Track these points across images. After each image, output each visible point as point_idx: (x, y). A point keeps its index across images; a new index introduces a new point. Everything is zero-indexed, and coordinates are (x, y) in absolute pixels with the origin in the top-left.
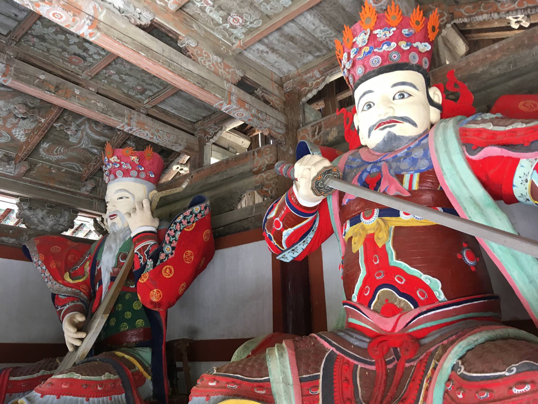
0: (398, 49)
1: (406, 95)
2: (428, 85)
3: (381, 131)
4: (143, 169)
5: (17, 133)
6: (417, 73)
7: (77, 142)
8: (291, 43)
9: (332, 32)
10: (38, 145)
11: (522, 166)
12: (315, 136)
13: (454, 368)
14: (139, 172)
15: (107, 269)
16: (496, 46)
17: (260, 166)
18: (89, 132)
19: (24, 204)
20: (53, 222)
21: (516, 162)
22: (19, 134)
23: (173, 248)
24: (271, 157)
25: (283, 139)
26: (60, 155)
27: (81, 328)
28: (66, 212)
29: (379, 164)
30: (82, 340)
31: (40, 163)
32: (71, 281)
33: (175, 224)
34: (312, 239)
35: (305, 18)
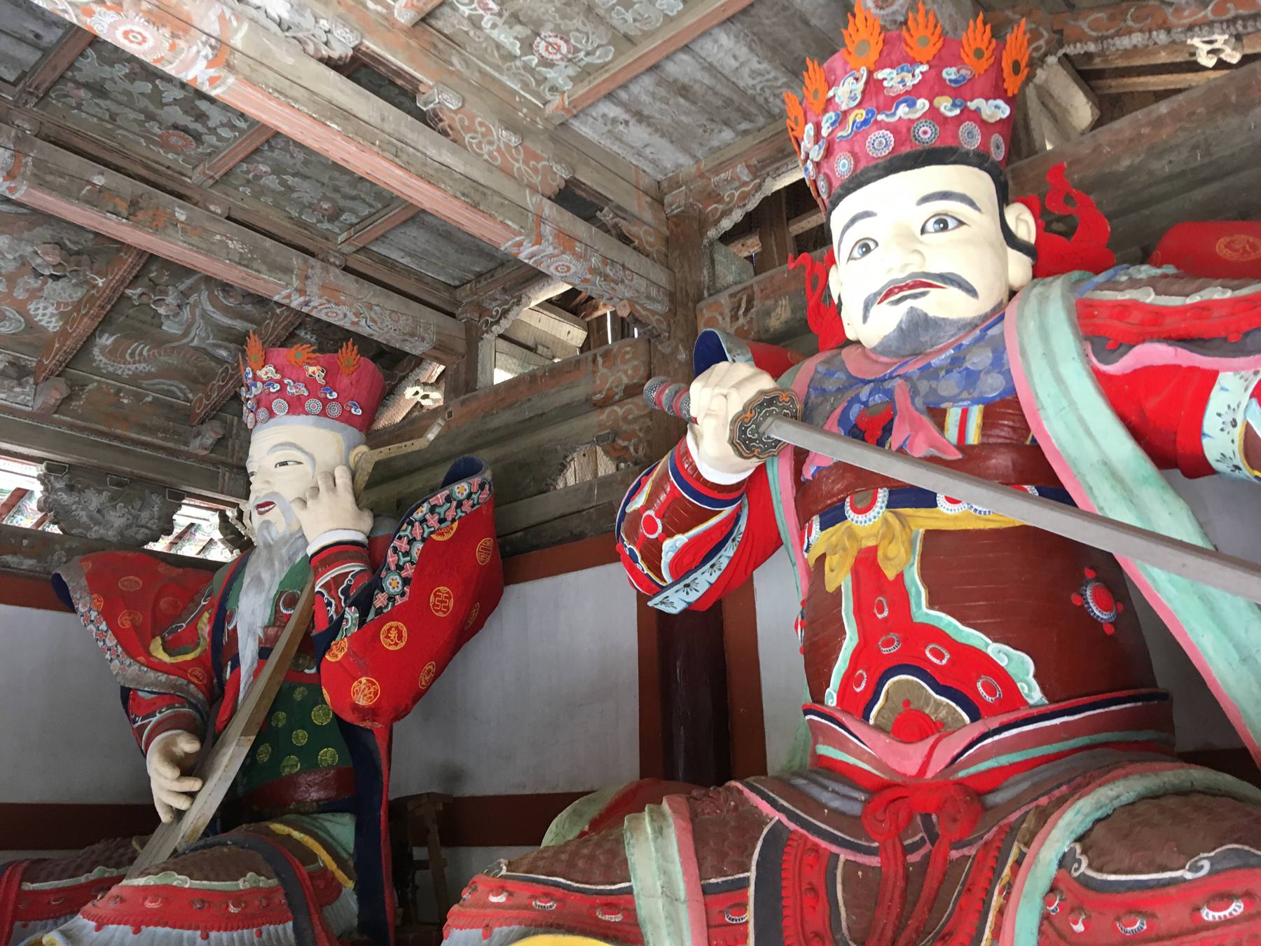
0: (933, 114)
1: (951, 224)
2: (1004, 199)
3: (894, 307)
4: (335, 395)
5: (40, 312)
6: (976, 170)
7: (179, 332)
8: (682, 101)
9: (779, 75)
10: (90, 340)
11: (1222, 389)
12: (737, 319)
13: (1065, 862)
14: (325, 402)
15: (251, 631)
16: (1163, 108)
17: (610, 389)
18: (209, 308)
19: (56, 478)
20: (123, 520)
21: (1209, 379)
22: (44, 315)
23: (406, 581)
24: (635, 369)
25: (664, 326)
26: (140, 362)
27: (190, 767)
28: (154, 497)
29: (888, 385)
30: (192, 795)
31: (93, 381)
32: (165, 658)
33: (411, 523)
34: (732, 560)
35: (716, 41)
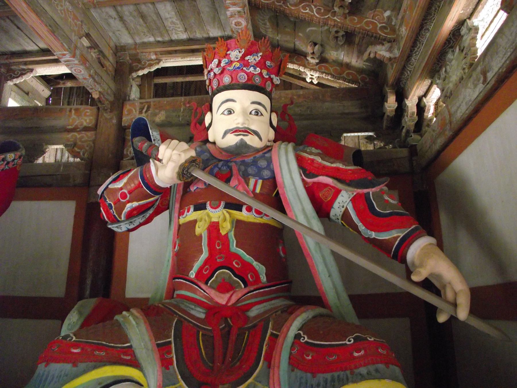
0: (261, 74)
1: (260, 114)
8: (141, 20)
9: (181, 27)
12: (142, 113)
13: (297, 337)
16: (301, 92)
17: (76, 126)
21: (338, 192)
24: (90, 120)
25: (109, 106)
29: (230, 164)
35: (165, 6)
